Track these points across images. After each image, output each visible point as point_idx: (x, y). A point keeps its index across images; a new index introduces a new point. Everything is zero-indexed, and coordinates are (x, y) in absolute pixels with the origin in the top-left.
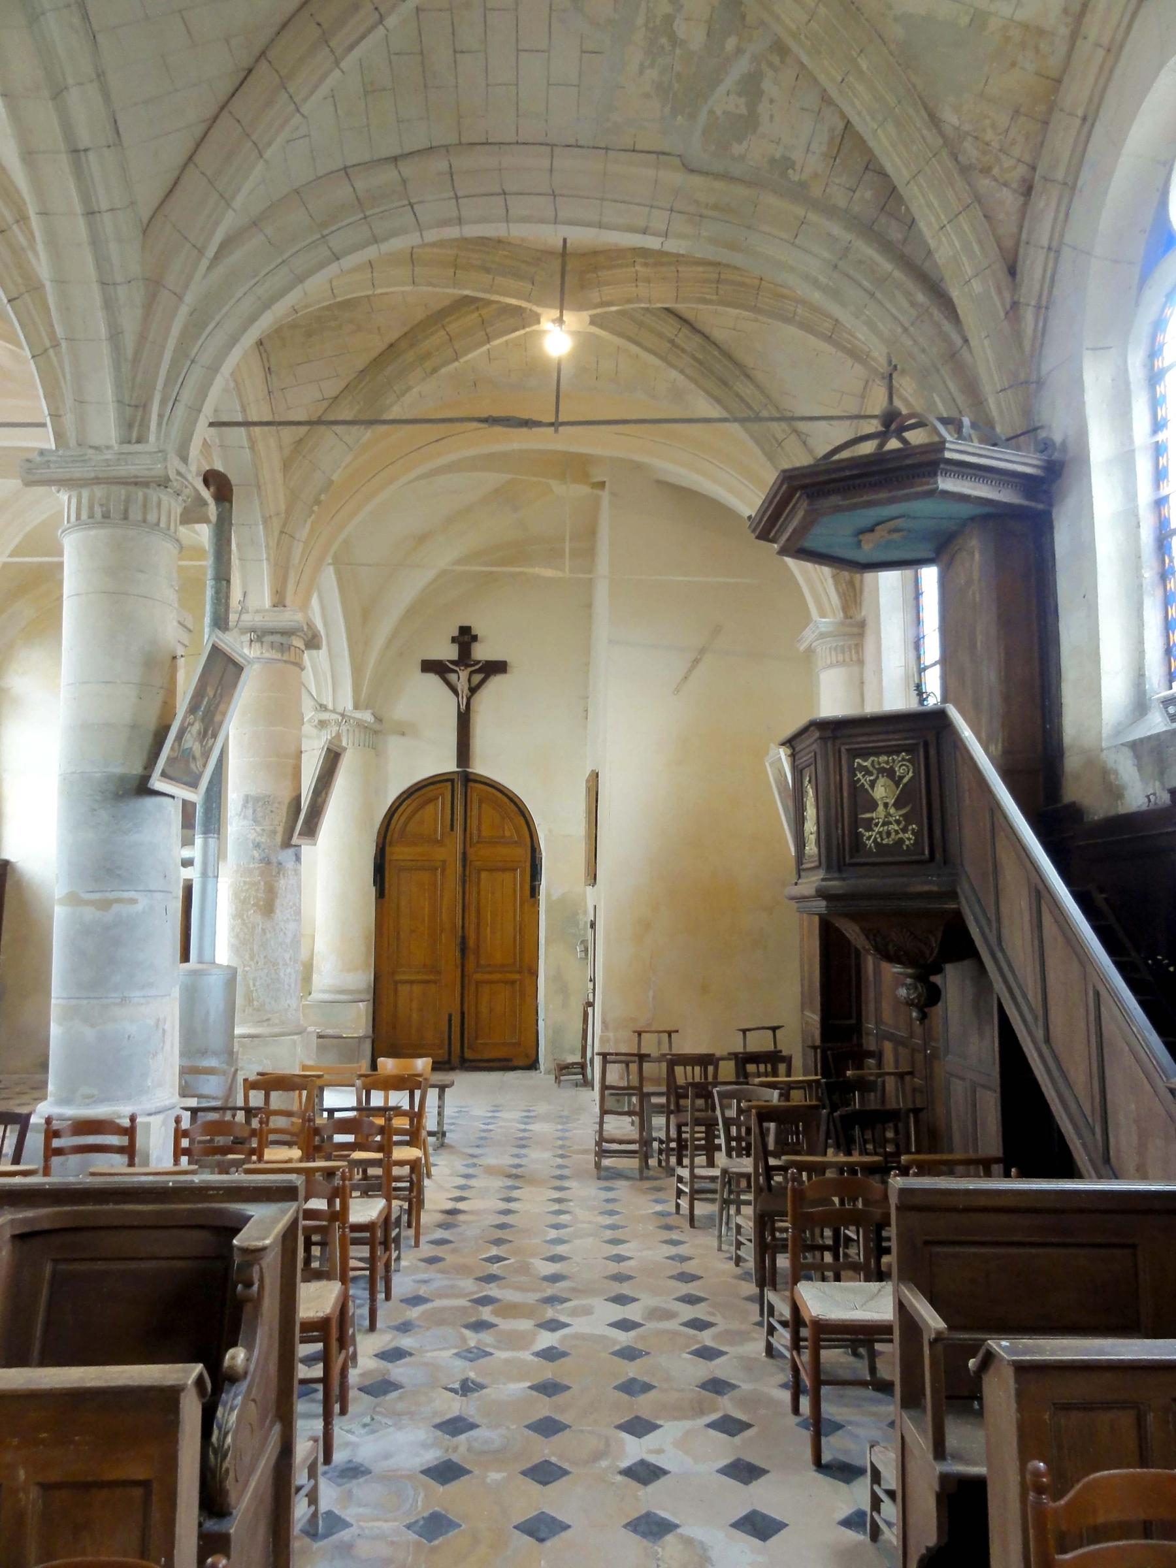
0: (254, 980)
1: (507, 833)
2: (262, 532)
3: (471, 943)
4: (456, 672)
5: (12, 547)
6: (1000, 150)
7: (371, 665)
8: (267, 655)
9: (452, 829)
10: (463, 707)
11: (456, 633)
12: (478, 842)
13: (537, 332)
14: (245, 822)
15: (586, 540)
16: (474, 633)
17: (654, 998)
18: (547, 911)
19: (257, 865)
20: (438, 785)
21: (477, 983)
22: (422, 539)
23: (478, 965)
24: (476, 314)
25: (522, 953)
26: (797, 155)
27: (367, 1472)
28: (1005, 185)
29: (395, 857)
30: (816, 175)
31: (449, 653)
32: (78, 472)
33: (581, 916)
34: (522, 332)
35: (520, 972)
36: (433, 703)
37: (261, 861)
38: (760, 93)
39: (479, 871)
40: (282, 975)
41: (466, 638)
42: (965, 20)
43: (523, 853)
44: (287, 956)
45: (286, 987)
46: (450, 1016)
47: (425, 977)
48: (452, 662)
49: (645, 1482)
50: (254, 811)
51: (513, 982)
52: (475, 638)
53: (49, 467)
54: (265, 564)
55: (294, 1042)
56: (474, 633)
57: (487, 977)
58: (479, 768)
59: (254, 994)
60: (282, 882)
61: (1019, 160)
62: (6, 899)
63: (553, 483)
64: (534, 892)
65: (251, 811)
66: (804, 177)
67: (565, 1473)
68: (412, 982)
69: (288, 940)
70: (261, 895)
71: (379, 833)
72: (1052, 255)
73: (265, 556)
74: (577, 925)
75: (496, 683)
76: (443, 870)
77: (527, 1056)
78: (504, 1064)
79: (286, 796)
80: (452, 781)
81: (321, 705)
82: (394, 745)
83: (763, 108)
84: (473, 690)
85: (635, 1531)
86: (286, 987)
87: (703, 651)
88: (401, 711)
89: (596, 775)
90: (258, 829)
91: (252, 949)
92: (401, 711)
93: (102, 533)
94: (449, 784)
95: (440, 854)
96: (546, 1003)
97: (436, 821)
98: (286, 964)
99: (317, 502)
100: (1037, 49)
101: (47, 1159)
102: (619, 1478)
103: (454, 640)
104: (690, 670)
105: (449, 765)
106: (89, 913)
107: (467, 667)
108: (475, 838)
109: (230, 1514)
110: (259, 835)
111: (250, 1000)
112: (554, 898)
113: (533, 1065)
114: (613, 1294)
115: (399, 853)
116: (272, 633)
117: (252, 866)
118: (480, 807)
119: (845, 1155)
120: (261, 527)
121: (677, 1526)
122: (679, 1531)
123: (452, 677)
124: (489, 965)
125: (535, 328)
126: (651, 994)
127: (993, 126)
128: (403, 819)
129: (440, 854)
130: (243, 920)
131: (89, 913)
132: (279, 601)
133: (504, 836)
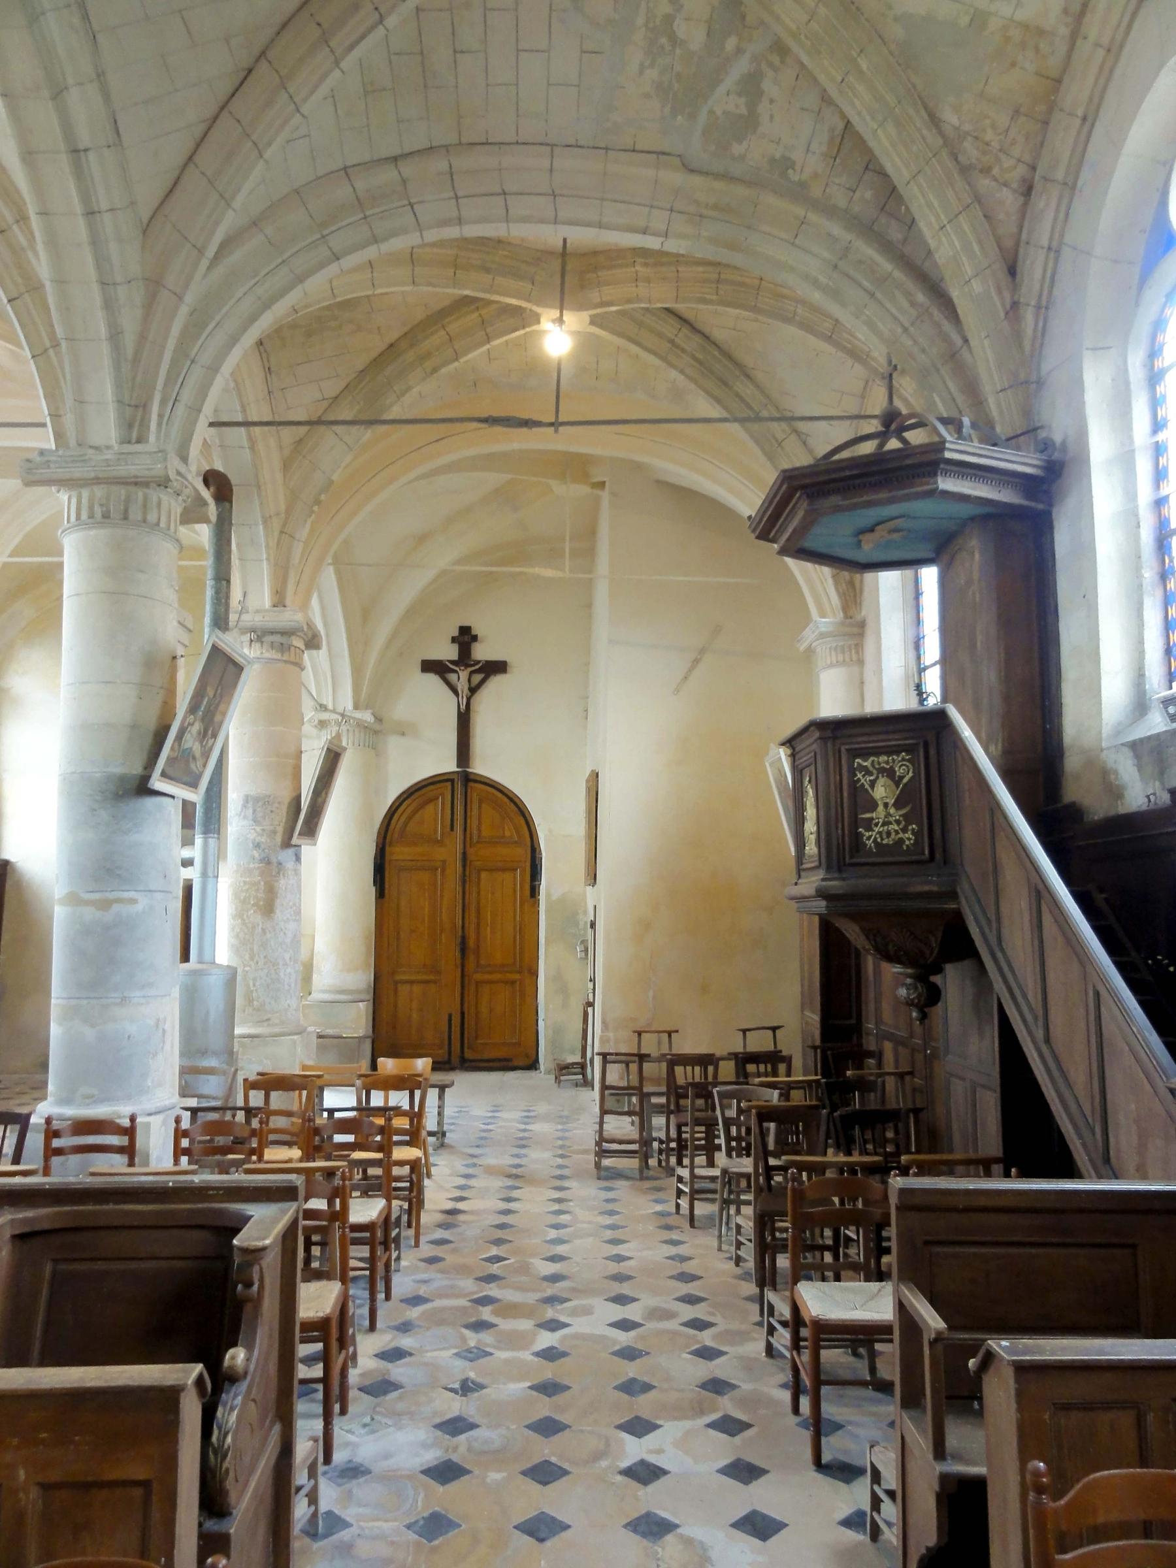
0: (254, 980)
1: (507, 833)
2: (262, 532)
3: (471, 943)
4: (456, 672)
5: (12, 547)
6: (1000, 150)
7: (371, 665)
8: (267, 655)
9: (452, 829)
10: (463, 707)
11: (456, 633)
12: (478, 842)
13: (537, 332)
14: (245, 822)
15: (586, 540)
16: (474, 633)
17: (654, 998)
18: (547, 911)
19: (257, 865)
20: (438, 785)
21: (477, 983)
22: (422, 539)
23: (478, 965)
24: (476, 314)
25: (522, 953)
26: (797, 155)
27: (367, 1472)
28: (1005, 185)
29: (395, 857)
30: (816, 175)
31: (449, 653)
32: (78, 472)
33: (581, 916)
34: (522, 332)
35: (520, 972)
36: (433, 703)
37: (261, 861)
38: (760, 93)
39: (479, 871)
40: (282, 975)
41: (466, 638)
42: (965, 20)
43: (523, 853)
44: (287, 956)
45: (286, 987)
46: (450, 1016)
47: (425, 977)
48: (452, 662)
49: (645, 1482)
50: (254, 811)
51: (513, 982)
52: (475, 638)
53: (49, 467)
54: (265, 564)
55: (294, 1042)
56: (474, 633)
57: (487, 977)
58: (479, 768)
59: (254, 994)
60: (282, 882)
61: (1019, 160)
62: (6, 899)
63: (553, 483)
64: (534, 892)
65: (251, 811)
66: (804, 177)
67: (565, 1473)
68: (412, 982)
69: (288, 940)
70: (261, 895)
71: (379, 833)
72: (1052, 255)
73: (265, 556)
74: (577, 925)
75: (496, 683)
76: (443, 870)
77: (527, 1056)
78: (504, 1064)
79: (286, 796)
80: (452, 781)
81: (321, 705)
82: (394, 745)
83: (763, 108)
84: (473, 690)
85: (635, 1531)
86: (286, 987)
87: (703, 651)
88: (401, 711)
89: (596, 775)
90: (258, 829)
91: (252, 949)
92: (401, 711)
93: (102, 533)
94: (449, 784)
95: (440, 854)
96: (546, 1003)
97: (436, 821)
98: (286, 964)
99: (317, 502)
100: (1037, 49)
101: (47, 1159)
102: (619, 1478)
103: (454, 640)
104: (690, 670)
105: (449, 765)
106: (89, 913)
107: (467, 667)
108: (475, 838)
109: (230, 1514)
110: (259, 835)
111: (250, 1000)
112: (554, 898)
113: (533, 1065)
114: (613, 1294)
115: (399, 853)
116: (272, 633)
117: (252, 866)
118: (480, 807)
119: (845, 1155)
120: (261, 527)
121: (677, 1526)
122: (679, 1531)
123: (452, 677)
124: (489, 965)
125: (535, 328)
126: (651, 994)
127: (993, 126)
128: (403, 819)
129: (440, 854)
130: (243, 920)
131: (89, 913)
132: (279, 601)
133: (504, 836)
